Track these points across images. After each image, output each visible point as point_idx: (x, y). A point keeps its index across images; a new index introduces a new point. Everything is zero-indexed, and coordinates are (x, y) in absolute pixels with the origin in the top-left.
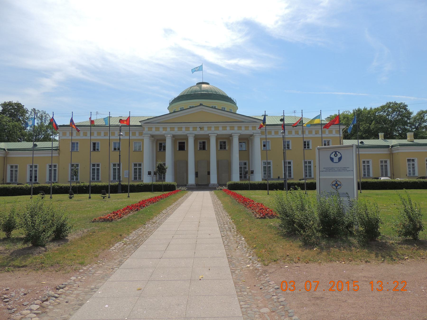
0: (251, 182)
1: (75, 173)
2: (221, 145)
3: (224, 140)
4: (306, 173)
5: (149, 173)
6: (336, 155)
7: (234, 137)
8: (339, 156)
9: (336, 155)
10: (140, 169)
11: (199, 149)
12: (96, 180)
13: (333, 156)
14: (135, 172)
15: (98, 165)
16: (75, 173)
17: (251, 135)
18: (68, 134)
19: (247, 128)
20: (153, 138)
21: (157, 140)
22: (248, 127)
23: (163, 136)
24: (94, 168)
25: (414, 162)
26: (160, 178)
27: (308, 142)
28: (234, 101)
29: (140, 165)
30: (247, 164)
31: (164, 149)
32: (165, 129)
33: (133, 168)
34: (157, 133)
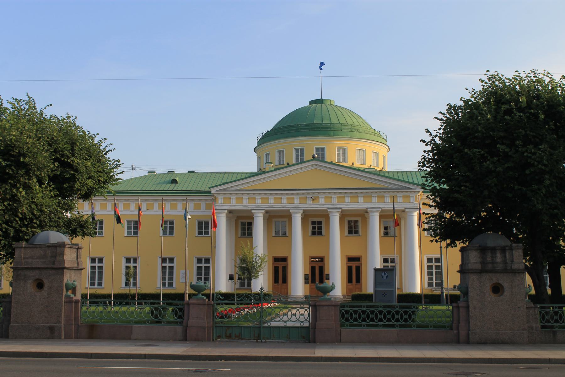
0: (364, 292)
1: (131, 276)
2: (350, 227)
3: (320, 219)
4: (432, 279)
5: (231, 278)
6: (385, 274)
7: (371, 214)
8: (387, 274)
9: (385, 274)
10: (207, 268)
11: (310, 233)
12: (131, 286)
13: (383, 275)
14: (93, 273)
15: (101, 261)
16: (131, 276)
17: (404, 211)
18: (203, 205)
19: (240, 200)
20: (231, 215)
21: (238, 218)
22: (294, 198)
23: (250, 211)
24: (128, 265)
25: (209, 263)
26: (242, 285)
27: (129, 232)
28: (382, 134)
29: (207, 261)
30: (397, 261)
31: (250, 234)
32: (252, 200)
33: (195, 265)
34: (239, 207)
